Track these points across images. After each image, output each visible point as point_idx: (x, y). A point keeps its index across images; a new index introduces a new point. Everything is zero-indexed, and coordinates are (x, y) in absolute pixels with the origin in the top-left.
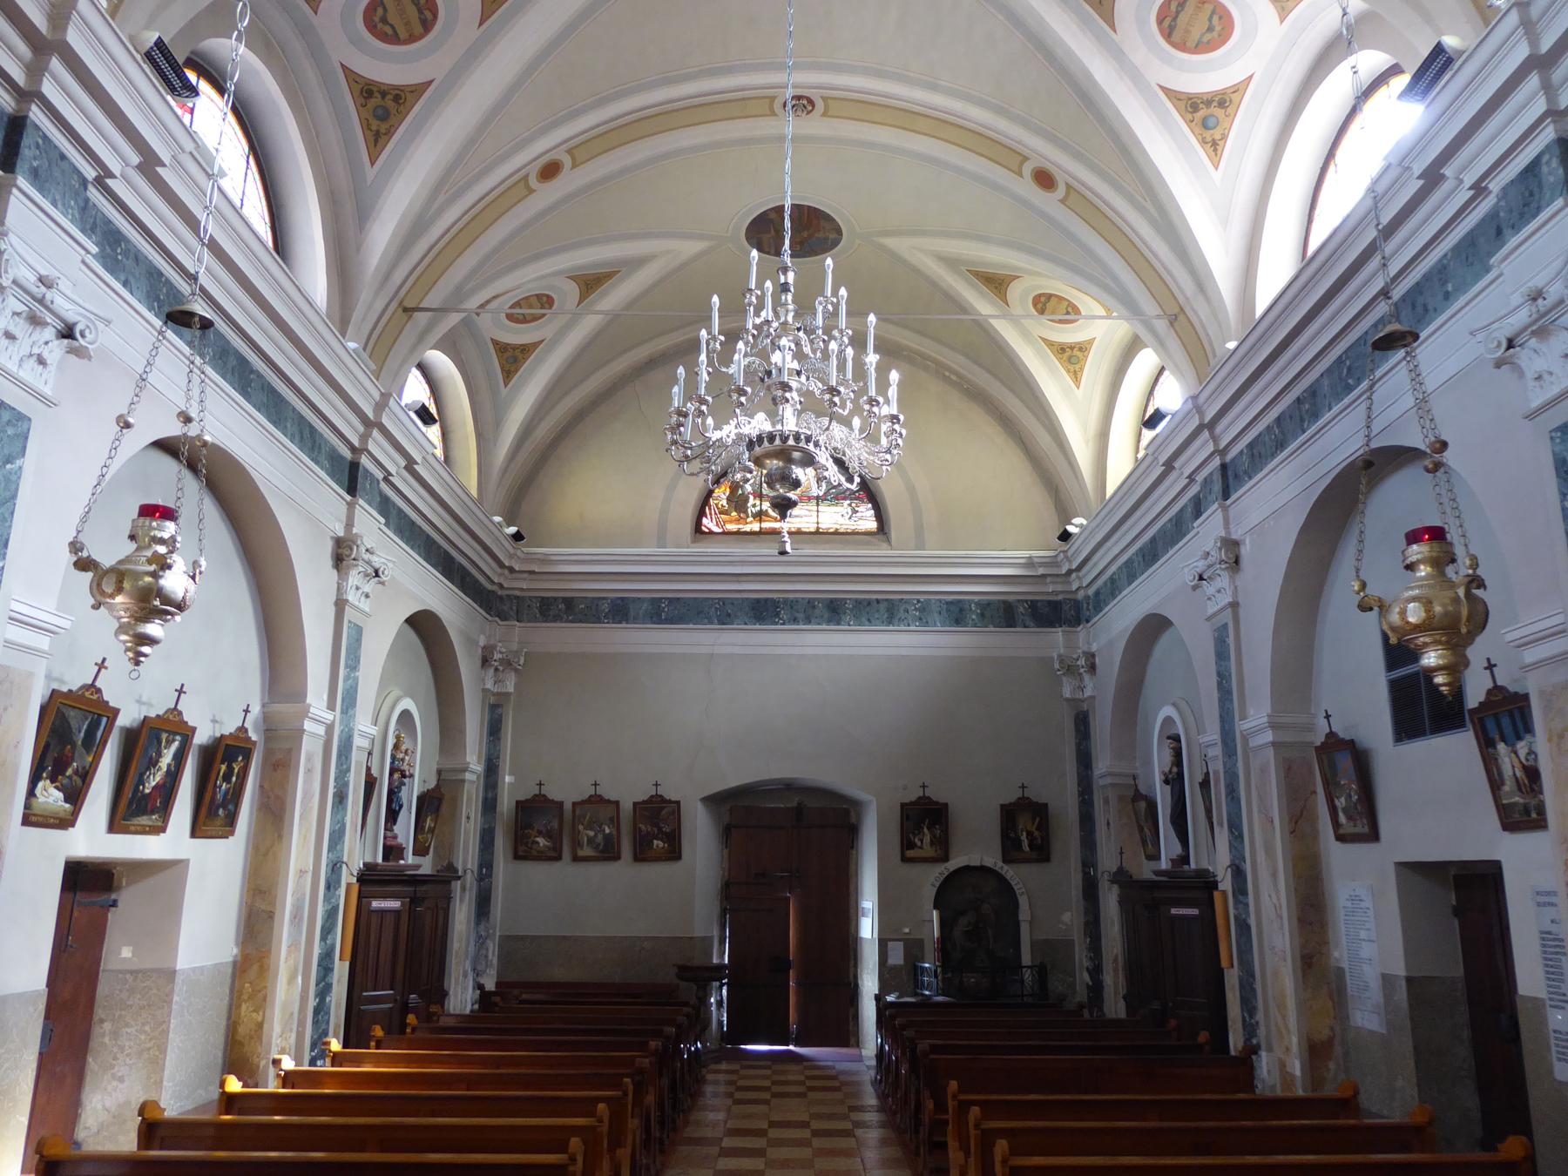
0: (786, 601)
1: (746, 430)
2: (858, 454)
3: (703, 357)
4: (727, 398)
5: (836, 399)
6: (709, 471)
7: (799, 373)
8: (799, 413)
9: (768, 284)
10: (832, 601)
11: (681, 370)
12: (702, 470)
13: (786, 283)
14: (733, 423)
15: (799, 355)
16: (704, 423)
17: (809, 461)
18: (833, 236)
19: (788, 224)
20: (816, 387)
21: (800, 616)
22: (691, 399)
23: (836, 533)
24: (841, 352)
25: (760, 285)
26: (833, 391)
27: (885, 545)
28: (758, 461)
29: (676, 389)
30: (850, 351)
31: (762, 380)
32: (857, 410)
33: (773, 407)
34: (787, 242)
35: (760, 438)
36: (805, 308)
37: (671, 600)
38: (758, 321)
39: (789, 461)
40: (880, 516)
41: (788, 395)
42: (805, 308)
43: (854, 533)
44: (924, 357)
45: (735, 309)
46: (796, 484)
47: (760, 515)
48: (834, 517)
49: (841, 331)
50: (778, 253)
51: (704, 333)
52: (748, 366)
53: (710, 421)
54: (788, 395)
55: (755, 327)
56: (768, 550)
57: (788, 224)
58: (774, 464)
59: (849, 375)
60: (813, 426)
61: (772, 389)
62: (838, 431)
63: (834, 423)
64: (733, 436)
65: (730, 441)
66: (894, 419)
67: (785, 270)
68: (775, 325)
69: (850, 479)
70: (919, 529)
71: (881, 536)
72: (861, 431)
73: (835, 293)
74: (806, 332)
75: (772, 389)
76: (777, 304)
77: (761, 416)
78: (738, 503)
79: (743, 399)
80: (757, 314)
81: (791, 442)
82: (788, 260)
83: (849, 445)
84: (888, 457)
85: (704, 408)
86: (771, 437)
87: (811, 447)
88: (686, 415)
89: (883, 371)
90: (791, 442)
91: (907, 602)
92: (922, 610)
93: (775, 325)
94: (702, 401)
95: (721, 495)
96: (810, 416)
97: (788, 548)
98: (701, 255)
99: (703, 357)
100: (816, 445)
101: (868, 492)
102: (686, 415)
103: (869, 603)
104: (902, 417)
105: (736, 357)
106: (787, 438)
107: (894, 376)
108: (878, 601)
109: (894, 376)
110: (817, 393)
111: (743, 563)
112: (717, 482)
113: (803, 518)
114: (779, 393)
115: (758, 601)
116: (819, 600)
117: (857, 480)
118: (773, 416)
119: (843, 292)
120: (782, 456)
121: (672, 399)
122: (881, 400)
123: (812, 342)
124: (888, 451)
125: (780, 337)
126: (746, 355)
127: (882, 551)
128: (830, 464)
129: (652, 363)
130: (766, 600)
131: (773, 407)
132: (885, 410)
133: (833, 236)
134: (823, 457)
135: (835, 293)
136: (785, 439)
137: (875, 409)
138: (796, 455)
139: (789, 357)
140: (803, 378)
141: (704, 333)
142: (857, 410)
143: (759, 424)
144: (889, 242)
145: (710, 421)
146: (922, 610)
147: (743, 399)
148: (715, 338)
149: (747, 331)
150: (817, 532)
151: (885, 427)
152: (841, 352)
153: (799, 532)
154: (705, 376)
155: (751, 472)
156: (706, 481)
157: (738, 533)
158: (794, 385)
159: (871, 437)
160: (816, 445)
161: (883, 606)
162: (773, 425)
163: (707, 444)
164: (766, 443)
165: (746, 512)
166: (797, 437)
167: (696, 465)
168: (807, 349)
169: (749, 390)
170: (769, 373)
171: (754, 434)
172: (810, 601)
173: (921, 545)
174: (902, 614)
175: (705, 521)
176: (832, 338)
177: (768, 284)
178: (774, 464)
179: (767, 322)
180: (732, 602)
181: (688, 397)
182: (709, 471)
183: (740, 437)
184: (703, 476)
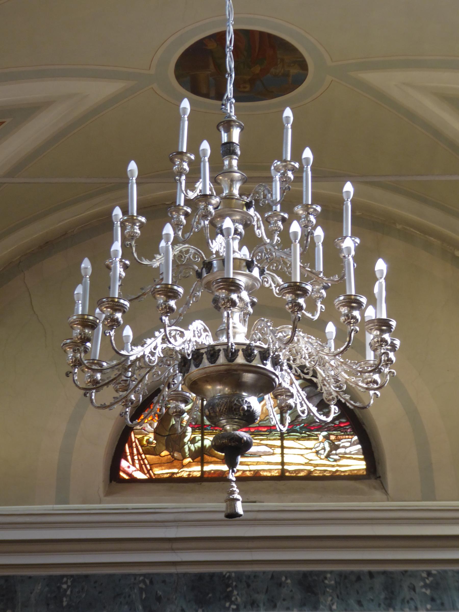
0: (239, 576)
1: (177, 344)
2: (334, 372)
3: (117, 246)
4: (151, 301)
5: (301, 301)
6: (126, 402)
7: (249, 265)
8: (250, 320)
9: (205, 145)
10: (305, 575)
11: (86, 264)
12: (116, 401)
13: (230, 143)
14: (159, 335)
15: (249, 239)
16: (119, 335)
17: (266, 385)
18: (294, 71)
19: (230, 63)
20: (274, 283)
21: (261, 597)
22: (100, 304)
23: (309, 477)
24: (307, 235)
25: (194, 146)
26: (297, 289)
27: (378, 494)
28: (194, 386)
29: (79, 290)
30: (319, 232)
31: (199, 275)
32: (330, 314)
33: (214, 313)
34: (230, 87)
35: (197, 355)
36: (256, 173)
37: (75, 579)
38: (192, 195)
39: (239, 385)
40: (370, 452)
41: (234, 296)
42: (256, 173)
43: (335, 477)
44: (425, 231)
45: (160, 172)
46: (248, 417)
47: (200, 455)
48: (303, 455)
49: (306, 207)
50: (220, 94)
51: (118, 212)
52: (178, 258)
53: (128, 331)
54: (234, 296)
55: (188, 202)
56: (214, 505)
57: (230, 63)
58: (218, 390)
59: (320, 267)
60: (273, 337)
61: (212, 289)
62: (305, 344)
63: (300, 334)
64: (159, 353)
65: (155, 359)
66: (382, 325)
67: (228, 125)
68: (215, 200)
69: (323, 406)
70: (426, 469)
71: (373, 482)
72: (339, 339)
73: (297, 155)
74: (257, 209)
75: (212, 289)
76: (217, 171)
77: (198, 325)
78: (170, 438)
79: (172, 303)
80: (191, 185)
81: (240, 360)
82: (231, 109)
83: (323, 364)
84: (376, 377)
85: (119, 315)
86: (213, 353)
87: (269, 366)
88: (93, 326)
89: (365, 258)
90: (240, 360)
91: (413, 575)
92: (435, 586)
93: (215, 200)
94: (117, 307)
95: (147, 430)
96: (266, 324)
97: (239, 508)
98: (113, 100)
99: (117, 246)
100: (276, 362)
101: (354, 420)
102: (93, 326)
103: (359, 577)
104: (393, 323)
105: (163, 244)
106: (234, 354)
107: (381, 266)
108: (371, 574)
109: (381, 266)
110: (276, 291)
111: (177, 523)
112: (139, 411)
113: (262, 458)
114: (222, 294)
115: (200, 577)
116: (288, 575)
117: (334, 410)
118: (218, 327)
119: (308, 153)
120: (229, 379)
121: (73, 303)
122: (364, 300)
123: (267, 221)
124: (377, 369)
125: (223, 217)
126: (176, 242)
127: (375, 502)
128: (296, 388)
129: (47, 247)
130: (212, 575)
131: (214, 313)
132: (370, 313)
133: (294, 71)
134: (285, 379)
135: (297, 155)
136: (231, 355)
137: (356, 313)
138: (248, 377)
139: (235, 244)
140: (256, 272)
141: (118, 212)
142: (330, 314)
143: (195, 335)
144: (373, 78)
145: (128, 331)
146: (435, 586)
147: (172, 303)
148: (132, 221)
149: (178, 208)
150: (283, 477)
151: (370, 337)
152: (307, 235)
153: (257, 477)
154: (120, 271)
155: (186, 401)
156: (122, 415)
157: (172, 480)
158: (242, 281)
159: (351, 346)
160: (276, 362)
161: (378, 582)
162: (216, 336)
163: (124, 364)
164: (206, 362)
165: (181, 450)
166: (248, 352)
167: (108, 394)
168: (261, 232)
169: (181, 290)
170: (208, 266)
171: (189, 349)
172: (274, 576)
173: (430, 495)
174: (406, 593)
175: (124, 464)
176: (295, 217)
177: (205, 145)
178: (218, 390)
179: (205, 197)
180: (164, 579)
181: (97, 302)
182: (126, 402)
183: (169, 353)
184: (118, 408)
